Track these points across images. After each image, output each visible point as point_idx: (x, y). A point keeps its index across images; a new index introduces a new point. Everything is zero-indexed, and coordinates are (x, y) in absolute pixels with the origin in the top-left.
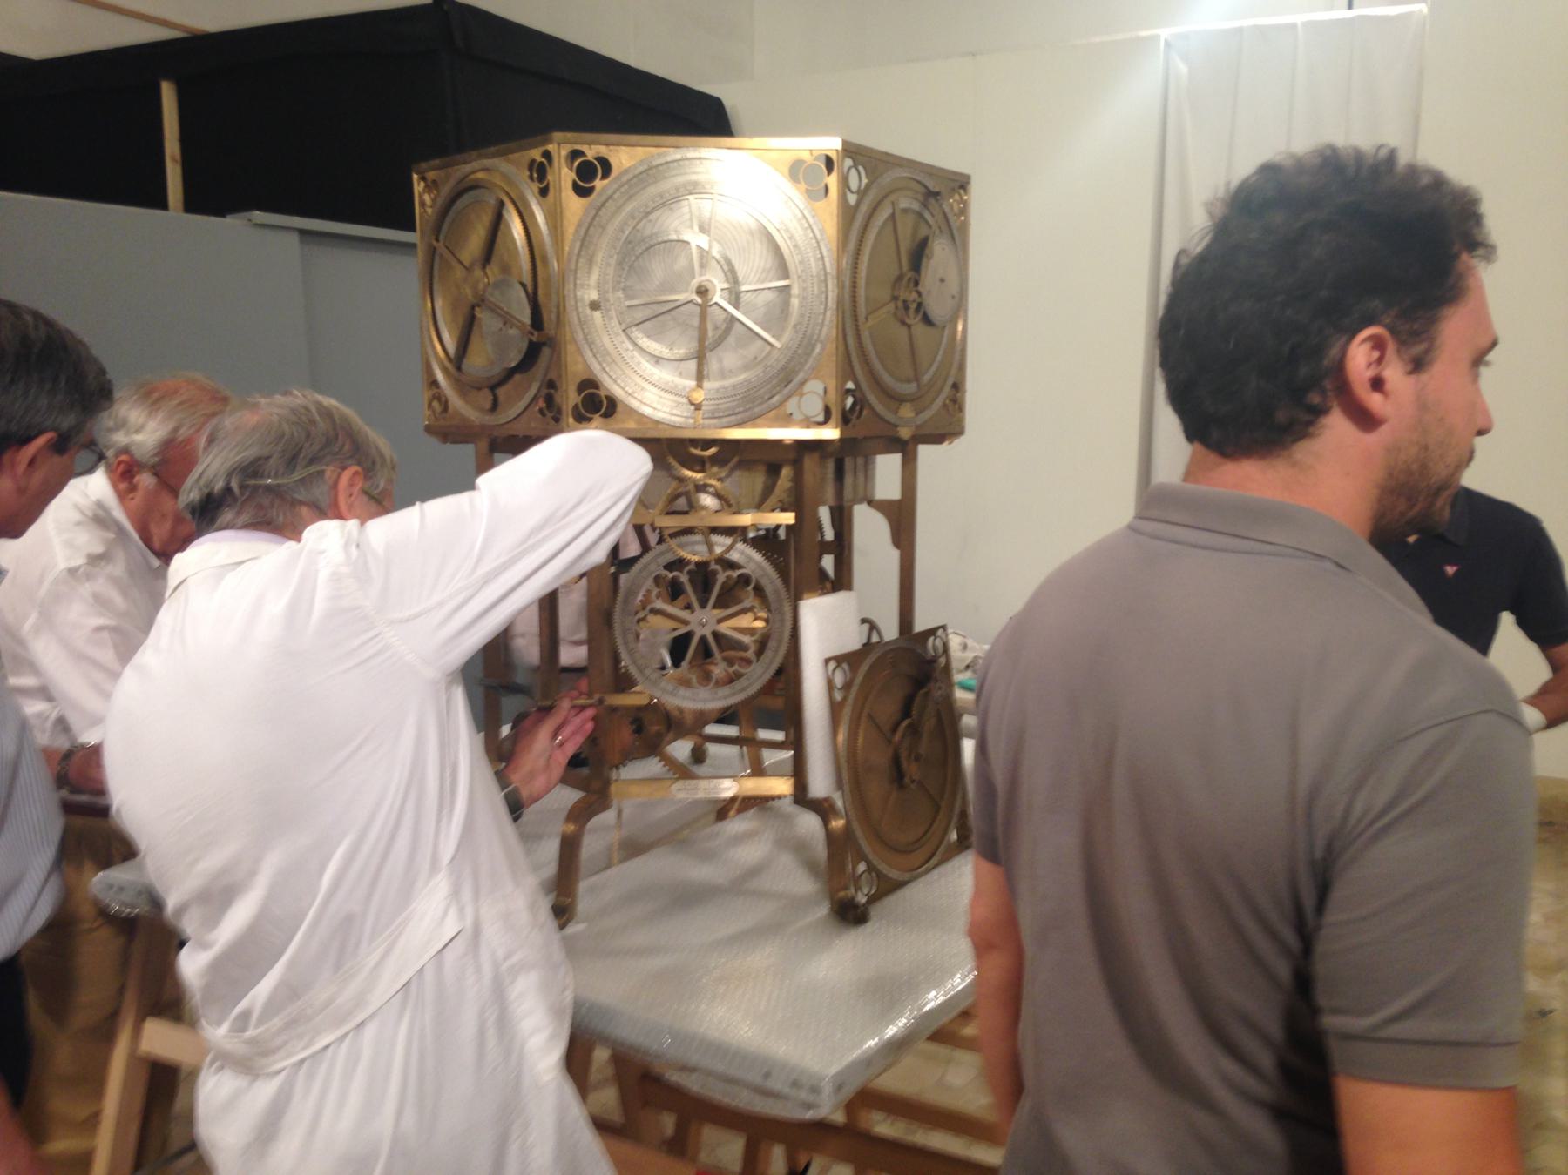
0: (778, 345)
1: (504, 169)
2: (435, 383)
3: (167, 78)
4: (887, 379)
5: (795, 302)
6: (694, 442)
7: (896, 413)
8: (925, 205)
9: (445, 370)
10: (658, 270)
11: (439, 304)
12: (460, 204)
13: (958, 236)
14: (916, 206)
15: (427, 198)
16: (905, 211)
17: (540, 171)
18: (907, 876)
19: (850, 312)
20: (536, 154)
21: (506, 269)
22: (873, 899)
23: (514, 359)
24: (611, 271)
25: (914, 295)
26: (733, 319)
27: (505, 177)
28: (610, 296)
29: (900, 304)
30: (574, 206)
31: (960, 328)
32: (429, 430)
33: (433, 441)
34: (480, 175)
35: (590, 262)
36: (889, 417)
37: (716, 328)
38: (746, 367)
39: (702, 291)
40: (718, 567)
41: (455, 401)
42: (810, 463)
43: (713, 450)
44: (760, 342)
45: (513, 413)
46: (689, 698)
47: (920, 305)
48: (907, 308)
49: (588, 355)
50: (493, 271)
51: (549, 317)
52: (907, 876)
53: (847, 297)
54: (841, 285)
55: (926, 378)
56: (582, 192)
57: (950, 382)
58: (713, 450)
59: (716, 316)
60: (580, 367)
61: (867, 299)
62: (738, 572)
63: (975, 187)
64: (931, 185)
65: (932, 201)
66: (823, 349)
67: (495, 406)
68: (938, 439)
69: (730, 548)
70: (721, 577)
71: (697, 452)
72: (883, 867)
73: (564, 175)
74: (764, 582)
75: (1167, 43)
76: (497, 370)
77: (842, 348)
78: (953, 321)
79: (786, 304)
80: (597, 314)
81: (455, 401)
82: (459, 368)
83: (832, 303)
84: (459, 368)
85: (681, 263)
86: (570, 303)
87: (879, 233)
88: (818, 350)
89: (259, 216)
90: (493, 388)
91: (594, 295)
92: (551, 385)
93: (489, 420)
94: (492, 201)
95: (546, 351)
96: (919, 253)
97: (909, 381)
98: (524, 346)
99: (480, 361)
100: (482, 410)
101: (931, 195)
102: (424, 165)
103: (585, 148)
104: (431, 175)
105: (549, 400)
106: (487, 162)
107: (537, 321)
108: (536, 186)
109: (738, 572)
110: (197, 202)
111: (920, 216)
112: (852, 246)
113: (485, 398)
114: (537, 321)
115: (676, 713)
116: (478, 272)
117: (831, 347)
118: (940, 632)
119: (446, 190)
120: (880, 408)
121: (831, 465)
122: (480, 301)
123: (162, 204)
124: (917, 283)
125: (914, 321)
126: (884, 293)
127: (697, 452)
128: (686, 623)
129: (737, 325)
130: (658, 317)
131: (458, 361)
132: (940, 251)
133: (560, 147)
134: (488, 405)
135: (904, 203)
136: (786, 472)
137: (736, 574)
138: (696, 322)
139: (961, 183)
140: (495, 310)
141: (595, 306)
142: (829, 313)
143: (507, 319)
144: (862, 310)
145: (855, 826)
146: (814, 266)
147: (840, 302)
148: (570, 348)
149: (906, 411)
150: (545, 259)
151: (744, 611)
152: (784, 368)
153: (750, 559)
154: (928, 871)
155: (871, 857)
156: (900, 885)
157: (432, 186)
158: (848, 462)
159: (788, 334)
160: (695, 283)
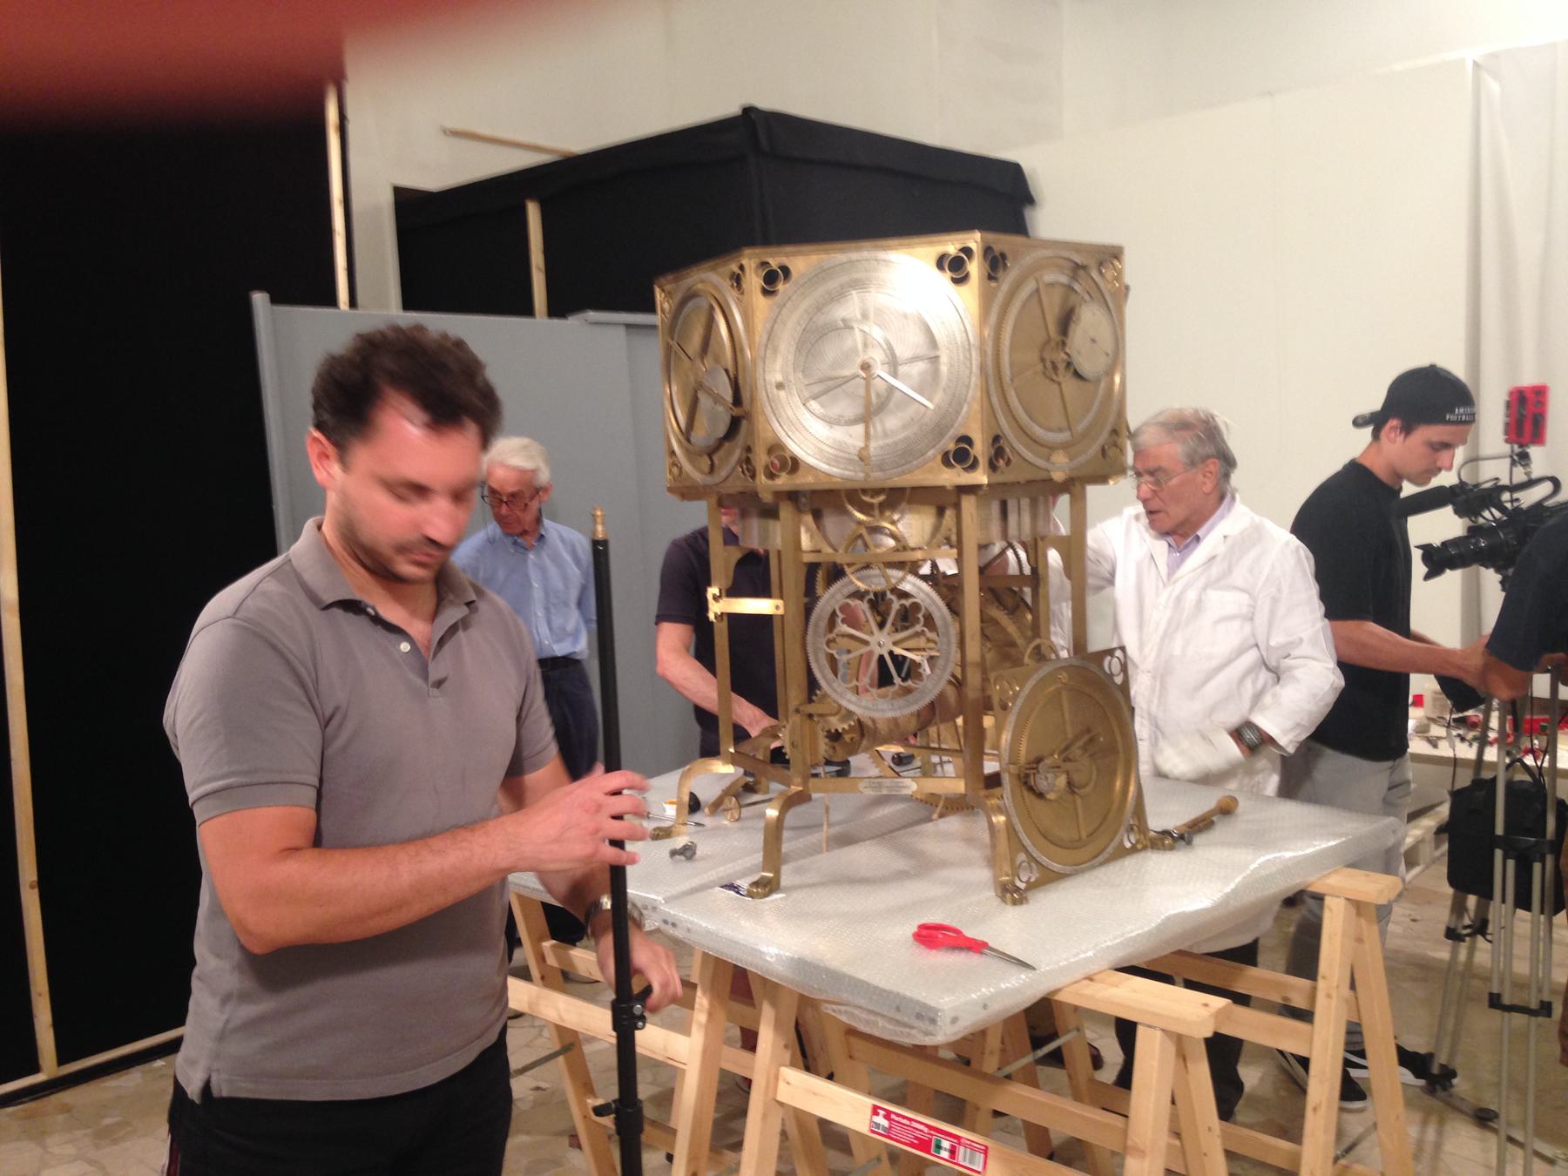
0: (931, 406)
1: (709, 278)
2: (673, 453)
3: (532, 198)
4: (1038, 431)
5: (944, 369)
6: (864, 491)
7: (1048, 459)
8: (1074, 277)
9: (679, 442)
10: (831, 350)
11: (674, 388)
12: (686, 310)
13: (1114, 301)
14: (1064, 279)
15: (666, 306)
16: (1052, 285)
17: (737, 280)
18: (1068, 869)
19: (993, 376)
20: (734, 268)
21: (717, 360)
22: (1032, 886)
23: (722, 430)
24: (791, 357)
25: (1064, 356)
26: (892, 389)
27: (716, 287)
28: (792, 378)
29: (1048, 364)
30: (761, 303)
31: (1117, 379)
32: (670, 490)
33: (673, 499)
34: (700, 286)
35: (775, 351)
36: (1039, 462)
37: (878, 395)
38: (905, 427)
39: (866, 367)
40: (893, 597)
41: (687, 467)
42: (968, 503)
43: (882, 498)
44: (916, 406)
45: (723, 474)
46: (877, 707)
47: (1069, 364)
48: (1055, 368)
49: (776, 426)
50: (709, 361)
51: (745, 395)
52: (1068, 869)
53: (990, 363)
54: (983, 353)
55: (1080, 427)
56: (767, 293)
57: (1108, 428)
58: (882, 498)
59: (878, 385)
60: (770, 434)
61: (1012, 364)
62: (911, 600)
63: (1128, 257)
64: (1078, 259)
65: (1081, 272)
66: (970, 407)
67: (712, 468)
68: (1102, 479)
69: (902, 579)
70: (896, 605)
71: (866, 499)
72: (1044, 860)
73: (754, 281)
74: (933, 610)
75: (1476, 64)
76: (712, 442)
77: (986, 403)
78: (1110, 373)
79: (936, 373)
80: (782, 393)
81: (687, 467)
82: (689, 441)
83: (975, 369)
84: (689, 441)
85: (849, 343)
86: (760, 383)
87: (1023, 306)
88: (965, 409)
89: (592, 315)
90: (710, 456)
91: (779, 378)
92: (749, 449)
93: (710, 480)
94: (706, 306)
95: (744, 423)
96: (1066, 321)
97: (1060, 430)
98: (728, 420)
99: (701, 435)
100: (701, 471)
101: (1077, 269)
102: (662, 280)
103: (771, 261)
104: (668, 287)
105: (748, 461)
106: (703, 275)
107: (737, 400)
108: (735, 293)
109: (911, 600)
110: (558, 309)
111: (1070, 288)
112: (993, 318)
113: (705, 462)
114: (737, 400)
115: (870, 723)
116: (698, 362)
117: (976, 406)
118: (1118, 653)
119: (678, 296)
120: (1029, 456)
121: (995, 508)
122: (700, 386)
123: (527, 310)
124: (1064, 344)
125: (1069, 384)
126: (1033, 356)
127: (866, 499)
128: (866, 643)
129: (897, 394)
130: (828, 387)
131: (687, 434)
132: (1090, 319)
133: (750, 261)
134: (706, 469)
135: (1049, 277)
136: (949, 513)
137: (907, 603)
138: (862, 392)
139: (1111, 255)
140: (710, 392)
141: (780, 386)
142: (974, 379)
143: (717, 399)
144: (1007, 372)
145: (1015, 820)
146: (959, 337)
147: (982, 368)
148: (761, 419)
149: (1060, 458)
150: (742, 350)
151: (917, 635)
152: (938, 425)
153: (920, 589)
154: (1093, 867)
155: (1031, 848)
156: (1059, 877)
157: (669, 294)
158: (1012, 505)
159: (939, 396)
160: (859, 361)
